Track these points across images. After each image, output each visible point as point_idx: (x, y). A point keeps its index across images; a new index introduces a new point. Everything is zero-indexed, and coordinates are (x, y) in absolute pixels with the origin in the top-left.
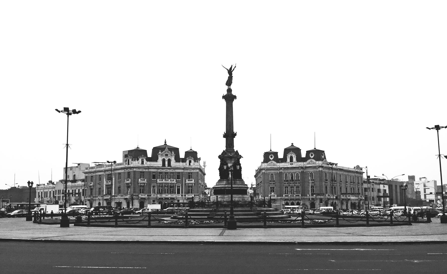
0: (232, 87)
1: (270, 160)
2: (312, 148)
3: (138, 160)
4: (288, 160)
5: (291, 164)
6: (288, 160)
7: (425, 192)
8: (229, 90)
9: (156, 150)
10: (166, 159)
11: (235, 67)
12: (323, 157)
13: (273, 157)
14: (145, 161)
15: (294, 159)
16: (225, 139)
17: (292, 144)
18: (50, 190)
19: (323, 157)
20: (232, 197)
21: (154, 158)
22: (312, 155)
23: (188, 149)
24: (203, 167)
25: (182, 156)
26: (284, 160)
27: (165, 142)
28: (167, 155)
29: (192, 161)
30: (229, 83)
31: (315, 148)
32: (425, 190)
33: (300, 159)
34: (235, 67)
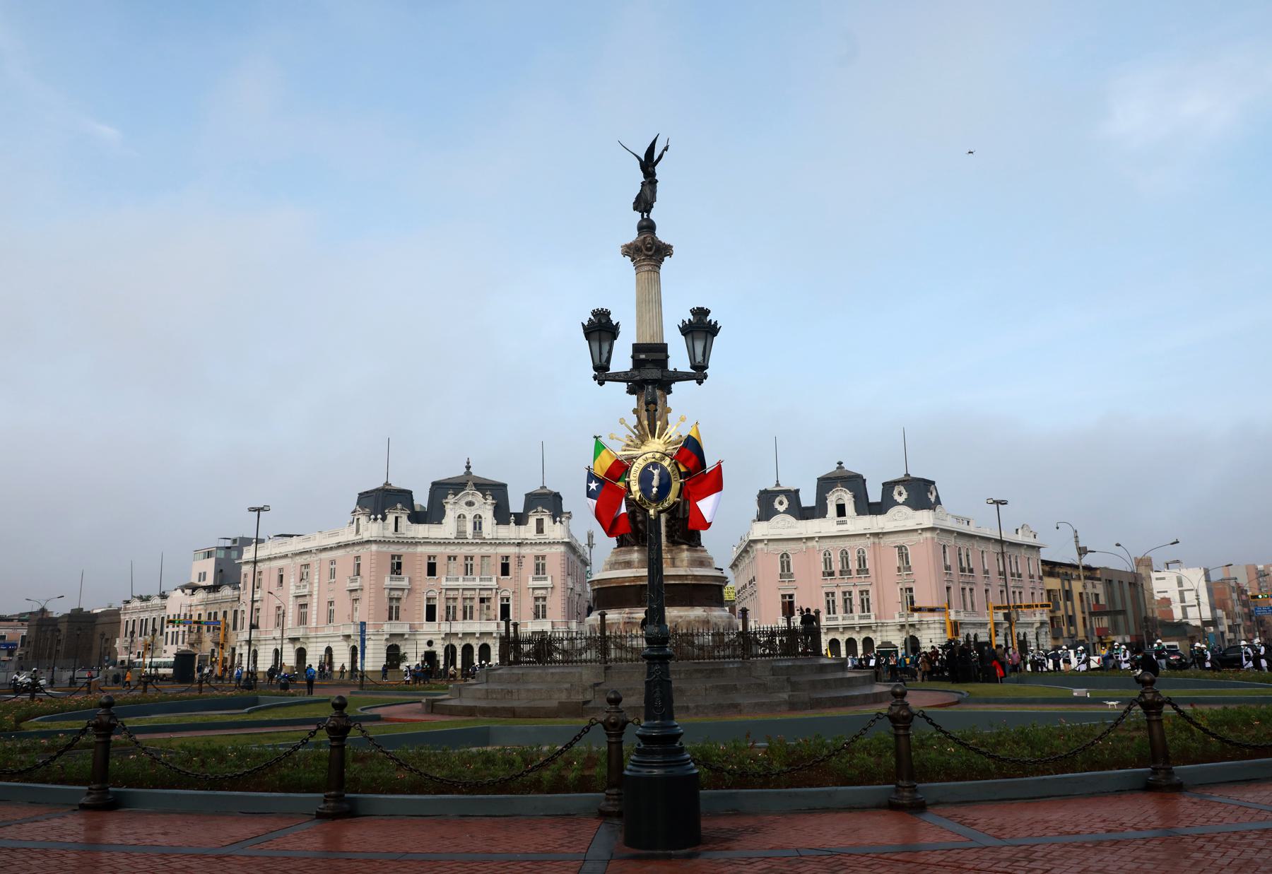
0: (654, 215)
1: (777, 512)
2: (900, 475)
3: (384, 519)
4: (832, 510)
5: (839, 523)
6: (832, 510)
7: (1183, 600)
8: (647, 227)
9: (441, 490)
10: (470, 517)
11: (666, 149)
12: (933, 499)
13: (786, 503)
14: (404, 520)
15: (850, 509)
16: (635, 397)
17: (840, 463)
18: (154, 615)
19: (933, 499)
20: (603, 616)
21: (433, 514)
22: (900, 494)
23: (534, 487)
24: (587, 549)
25: (516, 505)
26: (818, 511)
27: (468, 467)
28: (470, 504)
29: (547, 521)
30: (644, 203)
31: (907, 475)
32: (1181, 593)
33: (866, 508)
34: (666, 149)
